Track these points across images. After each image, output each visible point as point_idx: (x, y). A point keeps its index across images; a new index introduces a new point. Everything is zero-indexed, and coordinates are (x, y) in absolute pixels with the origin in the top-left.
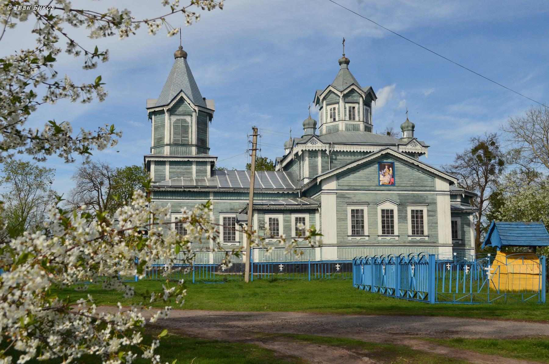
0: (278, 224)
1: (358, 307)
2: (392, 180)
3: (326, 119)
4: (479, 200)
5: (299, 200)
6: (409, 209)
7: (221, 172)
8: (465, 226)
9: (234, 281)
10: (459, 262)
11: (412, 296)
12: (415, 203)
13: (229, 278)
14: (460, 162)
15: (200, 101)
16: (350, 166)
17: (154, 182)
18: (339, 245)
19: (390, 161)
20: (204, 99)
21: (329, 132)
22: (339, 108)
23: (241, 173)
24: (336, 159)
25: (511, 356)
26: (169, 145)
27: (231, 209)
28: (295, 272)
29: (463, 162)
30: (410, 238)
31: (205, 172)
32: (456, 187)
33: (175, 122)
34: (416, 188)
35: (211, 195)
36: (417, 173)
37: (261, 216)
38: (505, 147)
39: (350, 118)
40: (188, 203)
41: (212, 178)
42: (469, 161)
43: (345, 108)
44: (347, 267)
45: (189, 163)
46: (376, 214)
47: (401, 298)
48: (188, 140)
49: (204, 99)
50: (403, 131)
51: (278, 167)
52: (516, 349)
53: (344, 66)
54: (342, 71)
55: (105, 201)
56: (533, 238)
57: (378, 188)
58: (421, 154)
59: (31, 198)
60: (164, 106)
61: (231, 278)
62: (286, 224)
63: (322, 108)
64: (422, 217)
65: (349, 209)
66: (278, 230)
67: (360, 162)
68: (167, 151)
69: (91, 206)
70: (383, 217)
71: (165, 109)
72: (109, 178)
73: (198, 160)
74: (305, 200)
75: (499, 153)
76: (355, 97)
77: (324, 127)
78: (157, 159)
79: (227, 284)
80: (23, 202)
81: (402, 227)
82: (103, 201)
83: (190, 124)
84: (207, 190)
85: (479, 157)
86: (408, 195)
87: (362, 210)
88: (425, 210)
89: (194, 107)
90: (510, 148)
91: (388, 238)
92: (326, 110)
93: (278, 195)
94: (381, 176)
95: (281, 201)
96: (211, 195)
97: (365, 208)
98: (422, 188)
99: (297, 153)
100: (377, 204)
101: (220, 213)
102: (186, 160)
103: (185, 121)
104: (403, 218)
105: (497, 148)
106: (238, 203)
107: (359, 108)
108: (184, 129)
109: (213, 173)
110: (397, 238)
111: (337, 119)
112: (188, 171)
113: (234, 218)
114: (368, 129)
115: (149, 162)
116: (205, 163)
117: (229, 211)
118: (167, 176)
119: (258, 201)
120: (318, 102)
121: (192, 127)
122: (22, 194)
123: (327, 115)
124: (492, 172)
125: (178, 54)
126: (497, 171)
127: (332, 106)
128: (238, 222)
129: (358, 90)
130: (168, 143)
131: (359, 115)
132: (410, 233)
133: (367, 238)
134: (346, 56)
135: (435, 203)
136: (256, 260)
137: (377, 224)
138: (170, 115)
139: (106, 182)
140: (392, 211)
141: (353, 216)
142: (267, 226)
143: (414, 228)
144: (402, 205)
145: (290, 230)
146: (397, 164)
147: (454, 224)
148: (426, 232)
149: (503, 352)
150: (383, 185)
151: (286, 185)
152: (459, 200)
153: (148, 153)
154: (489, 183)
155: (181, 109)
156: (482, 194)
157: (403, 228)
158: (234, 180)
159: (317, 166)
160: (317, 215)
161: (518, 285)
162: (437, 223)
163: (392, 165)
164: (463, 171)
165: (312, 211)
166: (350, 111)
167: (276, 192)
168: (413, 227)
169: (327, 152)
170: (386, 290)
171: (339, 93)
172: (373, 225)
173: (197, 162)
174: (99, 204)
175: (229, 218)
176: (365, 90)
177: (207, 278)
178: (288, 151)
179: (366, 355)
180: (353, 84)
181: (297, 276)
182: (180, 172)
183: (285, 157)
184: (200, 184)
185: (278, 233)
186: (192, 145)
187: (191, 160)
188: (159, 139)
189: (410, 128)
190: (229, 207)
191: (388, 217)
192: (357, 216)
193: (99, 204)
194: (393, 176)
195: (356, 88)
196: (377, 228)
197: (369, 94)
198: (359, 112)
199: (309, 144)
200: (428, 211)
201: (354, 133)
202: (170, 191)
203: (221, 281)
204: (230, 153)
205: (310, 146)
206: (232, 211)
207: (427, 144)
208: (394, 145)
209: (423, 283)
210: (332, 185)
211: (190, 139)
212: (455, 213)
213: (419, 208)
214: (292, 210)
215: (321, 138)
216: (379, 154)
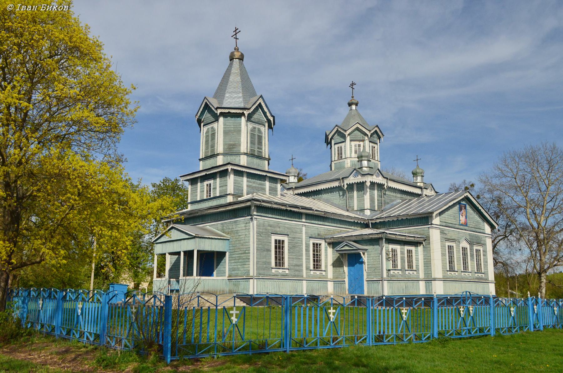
3: (351, 154)
22: (345, 146)
40: (285, 224)
48: (261, 152)
68: (244, 160)
83: (263, 135)
92: (335, 148)
96: (304, 216)
101: (310, 237)
103: (259, 130)
112: (262, 186)
117: (317, 237)
169: (385, 186)
173: (270, 178)
182: (255, 187)
186: (265, 159)
188: (230, 145)
214: (406, 242)
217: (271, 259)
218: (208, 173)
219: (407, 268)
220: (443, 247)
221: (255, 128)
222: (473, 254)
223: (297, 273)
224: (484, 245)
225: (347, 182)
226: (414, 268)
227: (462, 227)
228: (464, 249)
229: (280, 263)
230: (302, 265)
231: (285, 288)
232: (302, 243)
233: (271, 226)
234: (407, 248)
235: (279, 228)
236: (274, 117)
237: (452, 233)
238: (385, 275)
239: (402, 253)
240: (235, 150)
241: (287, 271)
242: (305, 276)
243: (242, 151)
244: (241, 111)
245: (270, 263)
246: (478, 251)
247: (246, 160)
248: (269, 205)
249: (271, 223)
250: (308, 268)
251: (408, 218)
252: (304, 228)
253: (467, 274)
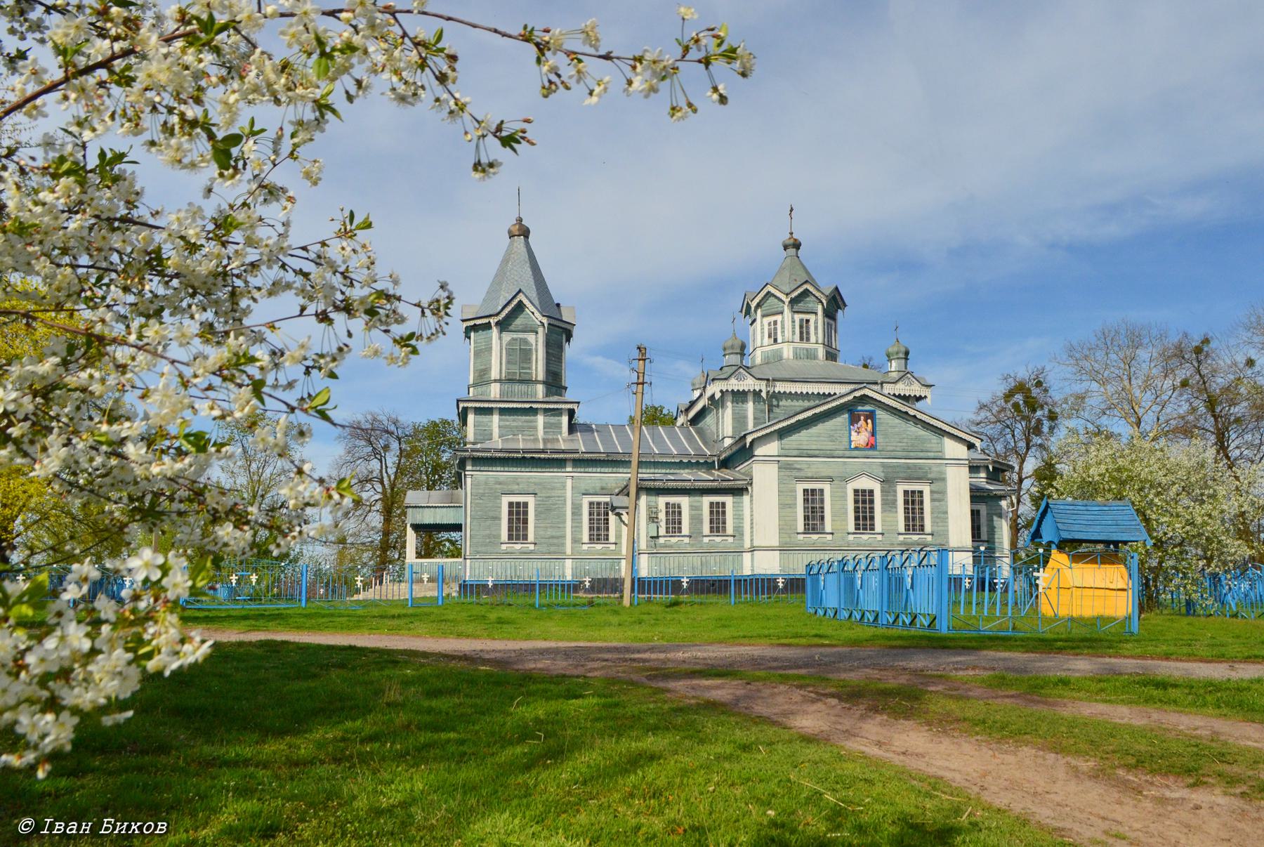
0: (680, 513)
1: (816, 636)
2: (872, 441)
4: (1015, 477)
5: (716, 473)
6: (901, 489)
7: (587, 428)
8: (995, 518)
9: (606, 604)
10: (984, 584)
11: (908, 622)
12: (909, 479)
13: (597, 601)
14: (983, 414)
15: (551, 308)
16: (801, 417)
17: (474, 444)
18: (783, 549)
19: (868, 408)
20: (558, 305)
21: (767, 362)
22: (782, 322)
23: (619, 428)
24: (778, 406)
25: (1096, 701)
26: (500, 381)
27: (602, 489)
28: (708, 592)
29: (988, 414)
30: (901, 538)
31: (559, 426)
32: (977, 455)
33: (509, 344)
34: (912, 454)
35: (569, 464)
36: (913, 429)
37: (653, 498)
38: (1061, 384)
39: (801, 339)
40: (530, 477)
41: (571, 437)
42: (999, 412)
43: (793, 322)
44: (795, 585)
45: (533, 412)
46: (844, 497)
47: (888, 626)
49: (558, 305)
50: (890, 360)
51: (681, 420)
52: (1102, 690)
53: (792, 251)
54: (788, 260)
55: (392, 477)
56: (1113, 528)
57: (848, 453)
58: (919, 399)
59: (268, 471)
60: (490, 316)
61: (601, 601)
63: (754, 321)
64: (922, 502)
65: (800, 488)
66: (680, 523)
67: (817, 410)
68: (495, 391)
69: (369, 486)
70: (856, 502)
72: (399, 439)
73: (547, 406)
74: (726, 474)
75: (1049, 400)
76: (810, 303)
77: (758, 353)
78: (478, 405)
79: (593, 609)
80: (256, 478)
82: (389, 476)
84: (561, 456)
85: (1016, 406)
86: (899, 466)
87: (822, 491)
88: (927, 490)
89: (540, 318)
90: (1068, 391)
91: (865, 537)
92: (762, 325)
93: (681, 465)
95: (686, 474)
96: (569, 464)
97: (827, 487)
98: (921, 454)
99: (713, 396)
100: (845, 480)
102: (527, 406)
103: (525, 341)
104: (889, 504)
105: (1046, 390)
106: (615, 478)
107: (816, 322)
108: (525, 355)
109: (572, 428)
110: (879, 538)
111: (779, 340)
113: (607, 504)
114: (831, 356)
115: (465, 410)
116: (558, 412)
117: (598, 491)
118: (494, 433)
119: (646, 474)
120: (748, 312)
122: (254, 466)
123: (762, 333)
124: (1037, 430)
125: (515, 230)
126: (1045, 429)
127: (772, 319)
128: (613, 509)
129: (815, 292)
131: (816, 333)
132: (902, 528)
133: (829, 537)
134: (795, 236)
135: (944, 480)
136: (644, 573)
137: (846, 513)
138: (501, 332)
139: (395, 445)
140: (871, 492)
141: (806, 500)
142: (662, 516)
144: (888, 483)
145: (701, 522)
146: (880, 414)
147: (975, 515)
148: (928, 528)
149: (1081, 694)
150: (856, 448)
151: (694, 449)
152: (983, 475)
153: (463, 396)
154: (1033, 449)
155: (519, 322)
156: (1021, 468)
157: (890, 520)
158: (607, 440)
159: (746, 417)
160: (746, 498)
161: (1087, 607)
162: (946, 513)
163: (871, 416)
164: (989, 430)
165: (738, 491)
166: (801, 327)
168: (907, 519)
169: (764, 394)
170: (863, 616)
171: (783, 297)
172: (839, 514)
174: (382, 482)
175: (599, 504)
176: (827, 293)
177: (560, 600)
178: (697, 393)
179: (833, 696)
180: (806, 282)
181: (712, 598)
183: (693, 403)
184: (549, 446)
185: (680, 529)
186: (537, 382)
187: (535, 406)
189: (902, 355)
190: (598, 485)
191: (864, 502)
192: (813, 502)
193: (382, 482)
194: (873, 434)
195: (811, 289)
196: (846, 520)
197: (834, 298)
198: (816, 328)
199: (733, 381)
200: (932, 492)
201: (808, 363)
202: (500, 458)
203: (584, 605)
204: (603, 400)
205: (734, 385)
206: (604, 491)
207: (930, 383)
208: (876, 383)
209: (925, 602)
210: (772, 448)
212: (977, 496)
213: (916, 487)
215: (751, 371)
216: (850, 397)
219: (706, 530)
224: (938, 480)
226: (730, 530)
230: (564, 537)
231: (529, 571)
234: (706, 500)
242: (569, 551)
244: (486, 321)
245: (499, 536)
248: (489, 455)
249: (501, 479)
250: (576, 541)
252: (569, 482)
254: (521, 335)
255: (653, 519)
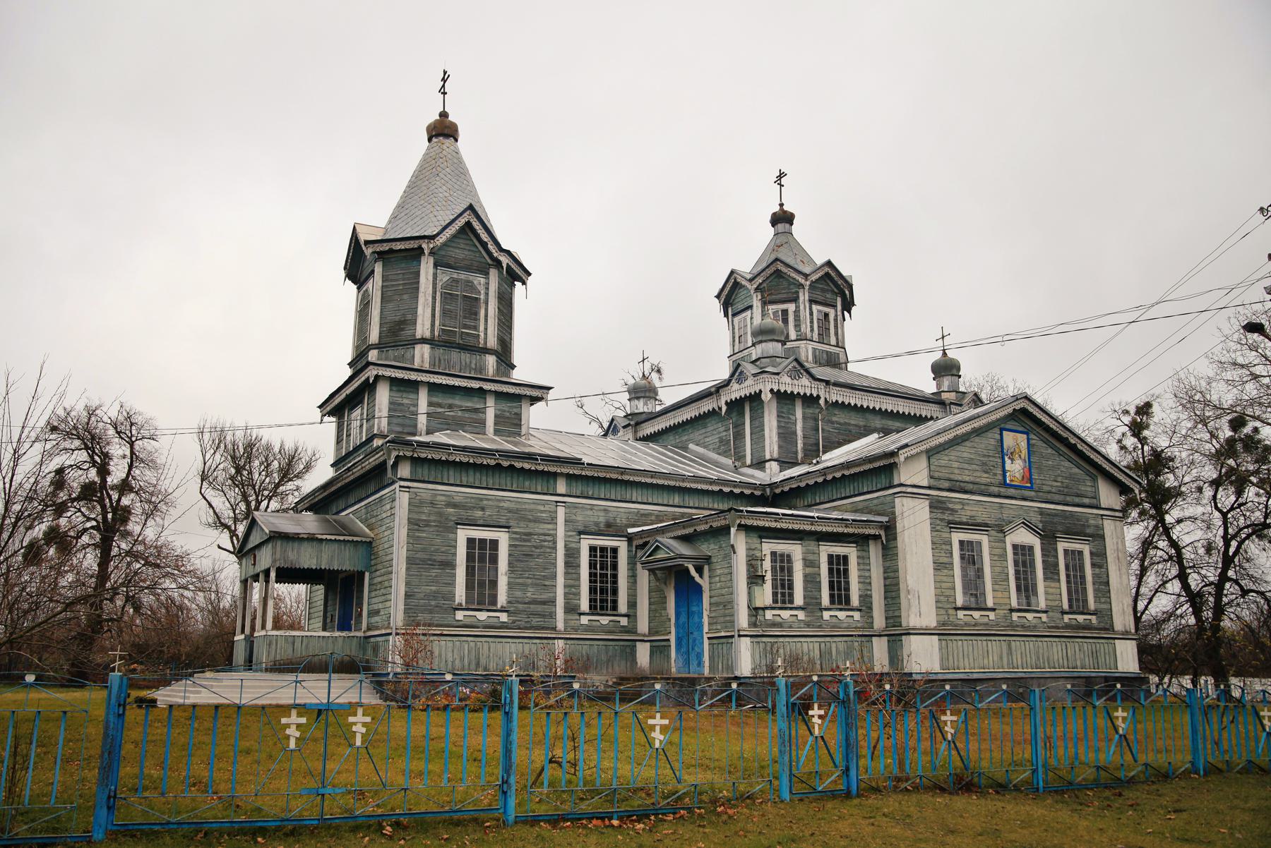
22: (797, 312)
30: (1066, 618)
34: (1068, 499)
40: (502, 499)
43: (811, 314)
62: (808, 570)
71: (424, 246)
81: (1051, 590)
94: (1008, 461)
101: (580, 533)
103: (470, 285)
104: (1051, 570)
121: (487, 304)
130: (427, 335)
135: (1103, 537)
140: (1031, 548)
143: (596, 593)
145: (818, 585)
159: (795, 433)
167: (716, 488)
169: (822, 402)
186: (486, 351)
211: (482, 335)
217: (453, 584)
218: (348, 392)
219: (826, 601)
220: (941, 545)
221: (456, 281)
222: (1057, 565)
223: (535, 621)
225: (726, 397)
226: (855, 601)
227: (1012, 492)
228: (1023, 552)
229: (839, 596)
230: (552, 602)
232: (555, 548)
233: (455, 506)
234: (826, 550)
235: (483, 509)
236: (508, 252)
237: (975, 506)
238: (743, 619)
239: (810, 563)
240: (407, 333)
241: (504, 617)
242: (560, 625)
243: (418, 336)
245: (452, 596)
246: (1074, 558)
247: (427, 356)
249: (457, 499)
250: (572, 609)
251: (847, 473)
252: (561, 512)
253: (1030, 616)
254: (463, 276)
255: (755, 579)
